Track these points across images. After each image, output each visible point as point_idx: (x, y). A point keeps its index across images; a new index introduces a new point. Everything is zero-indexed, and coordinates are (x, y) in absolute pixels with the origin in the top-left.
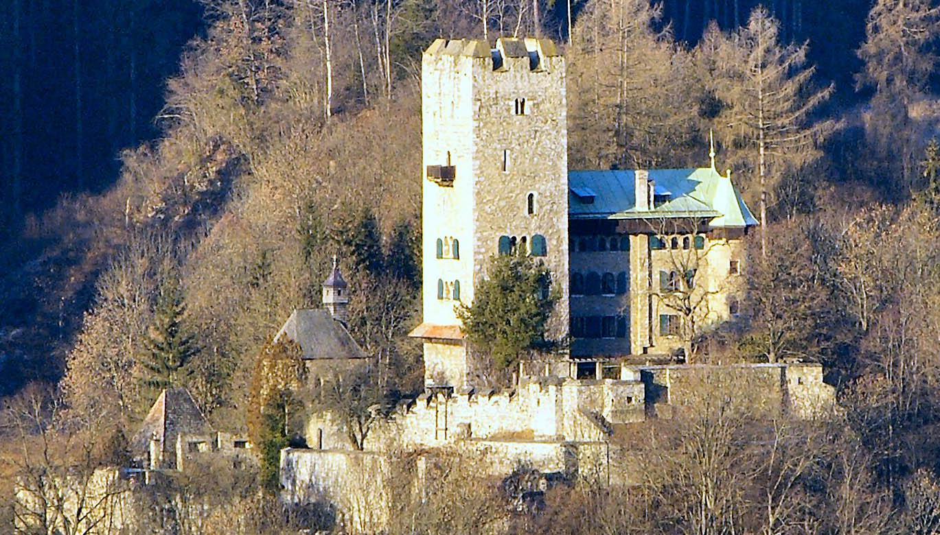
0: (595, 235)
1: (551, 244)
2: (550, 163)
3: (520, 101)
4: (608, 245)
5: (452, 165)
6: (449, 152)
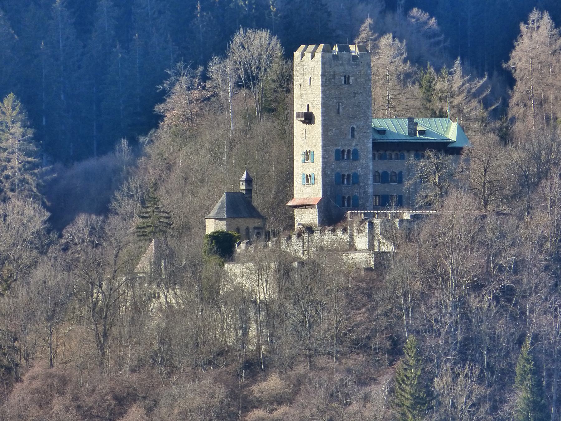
0: (386, 151)
1: (362, 154)
2: (363, 111)
3: (347, 76)
4: (393, 157)
5: (310, 111)
6: (308, 106)
